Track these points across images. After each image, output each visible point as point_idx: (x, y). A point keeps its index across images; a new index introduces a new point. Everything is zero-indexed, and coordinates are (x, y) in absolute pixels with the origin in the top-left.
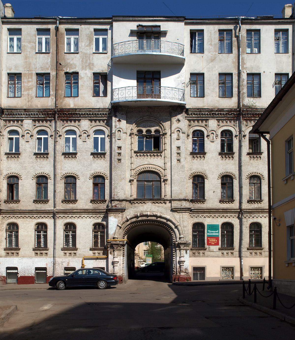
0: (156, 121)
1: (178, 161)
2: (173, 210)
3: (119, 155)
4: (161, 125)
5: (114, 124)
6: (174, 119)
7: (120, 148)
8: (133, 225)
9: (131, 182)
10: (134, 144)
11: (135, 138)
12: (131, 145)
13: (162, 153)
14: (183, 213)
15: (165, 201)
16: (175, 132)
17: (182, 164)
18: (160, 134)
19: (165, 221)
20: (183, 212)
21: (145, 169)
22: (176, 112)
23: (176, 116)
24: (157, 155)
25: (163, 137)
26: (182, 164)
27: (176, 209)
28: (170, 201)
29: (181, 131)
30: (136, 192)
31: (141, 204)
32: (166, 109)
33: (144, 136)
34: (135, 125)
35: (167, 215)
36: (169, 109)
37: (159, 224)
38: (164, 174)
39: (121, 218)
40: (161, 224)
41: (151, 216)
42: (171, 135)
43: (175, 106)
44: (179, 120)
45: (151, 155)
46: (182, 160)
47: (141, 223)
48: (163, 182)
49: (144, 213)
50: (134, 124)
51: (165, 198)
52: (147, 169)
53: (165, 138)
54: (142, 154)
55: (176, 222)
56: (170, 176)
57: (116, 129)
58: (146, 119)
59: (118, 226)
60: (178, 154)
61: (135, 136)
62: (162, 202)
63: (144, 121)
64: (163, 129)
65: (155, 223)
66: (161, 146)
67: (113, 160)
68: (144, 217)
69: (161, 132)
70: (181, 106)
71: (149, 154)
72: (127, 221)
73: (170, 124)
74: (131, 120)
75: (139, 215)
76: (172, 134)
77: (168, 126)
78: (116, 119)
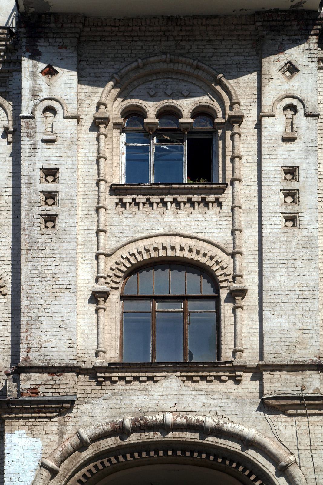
0: (200, 73)
1: (289, 224)
2: (269, 406)
3: (50, 201)
4: (219, 88)
5: (26, 84)
6: (272, 65)
7: (51, 173)
8: (107, 464)
9: (97, 302)
10: (109, 161)
11: (114, 139)
12: (98, 162)
13: (221, 191)
14: (311, 419)
15: (235, 372)
16: (278, 111)
17: (305, 232)
18: (216, 121)
19: (236, 447)
20: (309, 412)
21: (154, 254)
22: (281, 37)
23: (281, 50)
24: (203, 200)
25: (228, 133)
26: (305, 232)
27: (283, 402)
28: (257, 372)
29: (300, 106)
30: (118, 340)
31: (136, 383)
32: (239, 27)
33: (149, 132)
34: (114, 87)
35: (242, 423)
36: (252, 27)
37: (212, 458)
38: (230, 271)
39: (54, 437)
40: (220, 460)
41: (177, 427)
42: (259, 126)
43: (277, 11)
44: (292, 69)
45: (179, 200)
46: (305, 217)
47: (136, 455)
48: (225, 301)
49: (152, 418)
50: (111, 83)
51: (237, 362)
52: (162, 253)
53: (236, 136)
54: (141, 198)
55: (282, 452)
56: (257, 280)
57: (37, 101)
58: (158, 66)
59: (43, 465)
60: (291, 194)
61: (116, 132)
62: (224, 375)
63: (150, 74)
64: (228, 104)
65: (196, 455)
66: (221, 168)
67: (22, 220)
68: (152, 433)
69: (220, 115)
70: (304, 11)
71: (168, 198)
72: (83, 445)
73: (256, 85)
74: (97, 71)
75: (128, 423)
76: (265, 120)
77: (248, 91)
78: (35, 66)
